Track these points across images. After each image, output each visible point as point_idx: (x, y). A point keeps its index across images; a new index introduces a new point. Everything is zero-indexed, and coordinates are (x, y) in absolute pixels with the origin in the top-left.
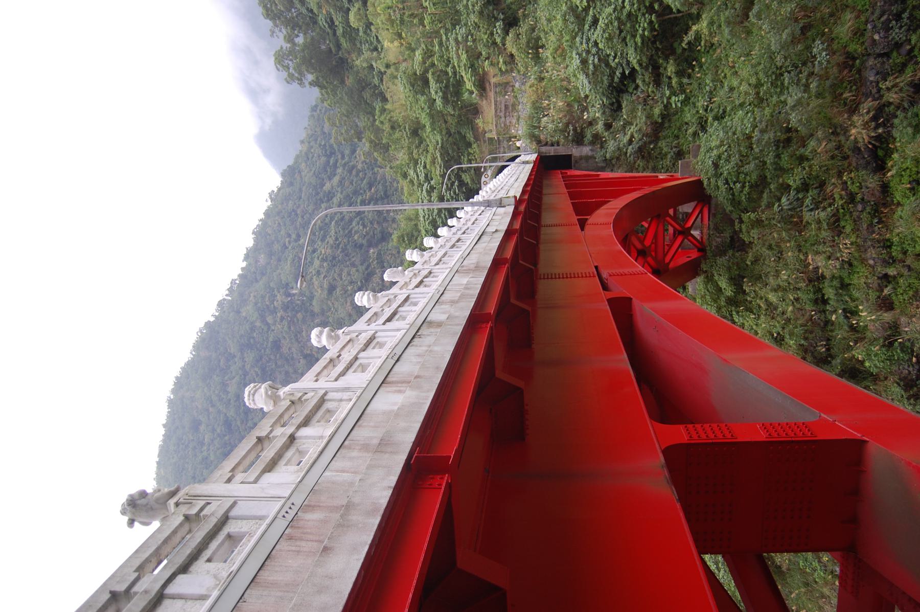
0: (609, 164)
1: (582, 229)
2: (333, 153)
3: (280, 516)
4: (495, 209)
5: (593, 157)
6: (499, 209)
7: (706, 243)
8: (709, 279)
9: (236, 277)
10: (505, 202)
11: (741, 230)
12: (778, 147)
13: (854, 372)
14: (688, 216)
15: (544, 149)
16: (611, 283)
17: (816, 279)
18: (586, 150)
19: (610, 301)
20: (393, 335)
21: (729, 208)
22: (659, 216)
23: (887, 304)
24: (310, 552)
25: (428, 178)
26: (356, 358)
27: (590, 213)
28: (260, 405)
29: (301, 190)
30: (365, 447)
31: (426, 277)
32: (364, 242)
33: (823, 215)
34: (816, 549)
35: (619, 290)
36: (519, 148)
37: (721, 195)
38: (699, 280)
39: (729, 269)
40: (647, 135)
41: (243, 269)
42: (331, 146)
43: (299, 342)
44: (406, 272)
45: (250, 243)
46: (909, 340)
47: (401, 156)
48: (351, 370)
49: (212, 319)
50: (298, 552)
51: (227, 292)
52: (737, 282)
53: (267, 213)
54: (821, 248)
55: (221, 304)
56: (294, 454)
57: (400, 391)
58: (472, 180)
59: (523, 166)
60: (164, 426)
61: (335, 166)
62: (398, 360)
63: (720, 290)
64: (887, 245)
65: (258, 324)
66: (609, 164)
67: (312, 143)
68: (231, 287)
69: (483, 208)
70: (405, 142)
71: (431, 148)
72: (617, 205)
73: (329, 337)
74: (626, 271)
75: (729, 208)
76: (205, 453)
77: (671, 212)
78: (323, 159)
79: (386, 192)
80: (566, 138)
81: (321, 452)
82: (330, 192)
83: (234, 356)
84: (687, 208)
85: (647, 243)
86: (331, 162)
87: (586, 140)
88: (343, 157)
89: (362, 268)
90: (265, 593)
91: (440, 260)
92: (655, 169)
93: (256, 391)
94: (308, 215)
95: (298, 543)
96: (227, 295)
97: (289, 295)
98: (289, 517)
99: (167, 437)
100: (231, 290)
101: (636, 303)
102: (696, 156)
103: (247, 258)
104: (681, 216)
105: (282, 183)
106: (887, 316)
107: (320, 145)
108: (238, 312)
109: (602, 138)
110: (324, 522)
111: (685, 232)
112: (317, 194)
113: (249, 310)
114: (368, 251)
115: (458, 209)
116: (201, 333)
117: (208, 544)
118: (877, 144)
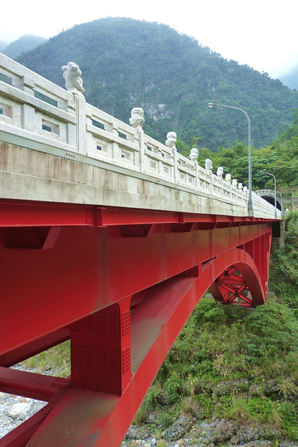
0: (275, 256)
1: (237, 248)
2: (288, 107)
3: (67, 152)
4: (247, 206)
5: (278, 248)
6: (247, 209)
7: (231, 305)
8: (213, 306)
9: (222, 56)
10: (251, 211)
11: (237, 322)
12: (279, 343)
13: (165, 373)
14: (245, 295)
15: (284, 223)
16: (207, 266)
17: (211, 358)
18: (282, 244)
19: (197, 266)
20: (170, 177)
21: (249, 317)
22: (245, 282)
23: (198, 391)
24: (49, 172)
25: (270, 161)
26: (158, 160)
27: (247, 250)
28: (132, 116)
29: (268, 90)
30: (107, 182)
31: (206, 182)
32: (239, 126)
33: (243, 364)
34: (72, 370)
35: (203, 270)
36: (285, 209)
37: (255, 313)
38: (213, 301)
39: (218, 315)
40: (289, 276)
41: (226, 60)
42: (292, 106)
43: (187, 92)
44: (210, 171)
45: (240, 63)
46: (180, 401)
47: (284, 147)
48: (151, 160)
49: (199, 44)
50: (48, 167)
51: (214, 52)
52: (212, 319)
53: (256, 72)
54: (227, 361)
55: (208, 48)
56: (104, 145)
57: (138, 189)
58: (269, 185)
59: (274, 214)
60: (143, 20)
61: (281, 109)
62: (156, 183)
63: (208, 310)
64: (227, 394)
65: (197, 70)
66: (275, 256)
67: (294, 96)
68: (217, 54)
69: (248, 200)
70: (291, 148)
71: (287, 163)
72: (250, 262)
73: (172, 142)
74: (213, 272)
75: (249, 317)
76: (130, 43)
77: (247, 288)
78: (284, 103)
79: (265, 137)
80: (289, 235)
81: (103, 162)
82: (266, 106)
83: (180, 57)
84: (249, 296)
85: (232, 277)
86: (283, 107)
87: (288, 245)
88: (285, 113)
89: (225, 125)
90: (26, 158)
91: (216, 187)
92: (270, 280)
93: (140, 114)
94: (254, 95)
95: (53, 165)
96: (212, 52)
97: (212, 86)
98: (67, 157)
99: (137, 22)
100: (215, 54)
101: (195, 280)
102: (276, 301)
103: (232, 62)
104: (246, 292)
105: (273, 80)
106: (192, 391)
107: (293, 100)
108: (203, 59)
109: (289, 253)
110: (65, 174)
111: (237, 294)
112: (266, 100)
113: (204, 64)
114: (234, 128)
115: (248, 187)
116: (192, 38)
117: (52, 117)
118: (279, 394)
